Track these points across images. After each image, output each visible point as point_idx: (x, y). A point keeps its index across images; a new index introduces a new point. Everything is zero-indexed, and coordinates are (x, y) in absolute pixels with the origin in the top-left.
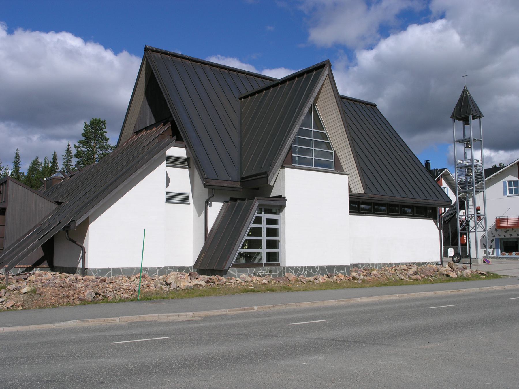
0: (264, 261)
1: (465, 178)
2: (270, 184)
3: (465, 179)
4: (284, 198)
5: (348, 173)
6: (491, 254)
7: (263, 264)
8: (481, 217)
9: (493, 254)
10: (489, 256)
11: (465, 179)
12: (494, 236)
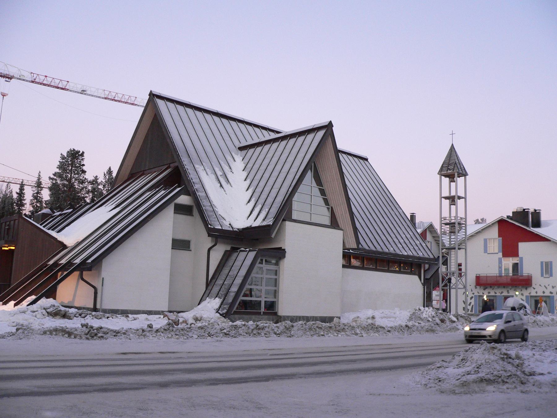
0: (263, 310)
1: (449, 230)
2: (272, 237)
3: (448, 231)
4: (284, 250)
5: (343, 229)
6: (470, 311)
7: (261, 312)
8: (463, 274)
9: (472, 311)
10: (468, 313)
11: (448, 231)
12: (473, 294)
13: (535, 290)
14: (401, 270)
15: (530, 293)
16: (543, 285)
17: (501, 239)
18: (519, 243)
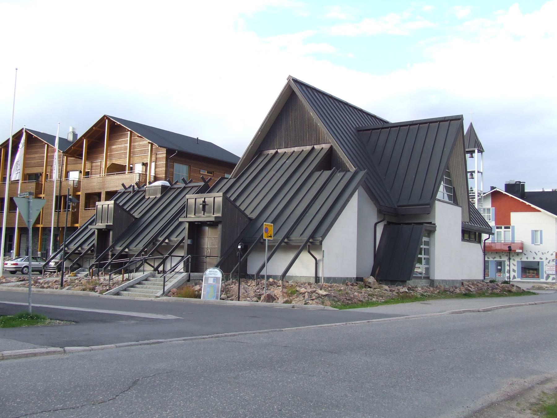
13: (526, 256)
14: (465, 238)
15: (521, 259)
16: (533, 252)
17: (494, 209)
18: (511, 213)
